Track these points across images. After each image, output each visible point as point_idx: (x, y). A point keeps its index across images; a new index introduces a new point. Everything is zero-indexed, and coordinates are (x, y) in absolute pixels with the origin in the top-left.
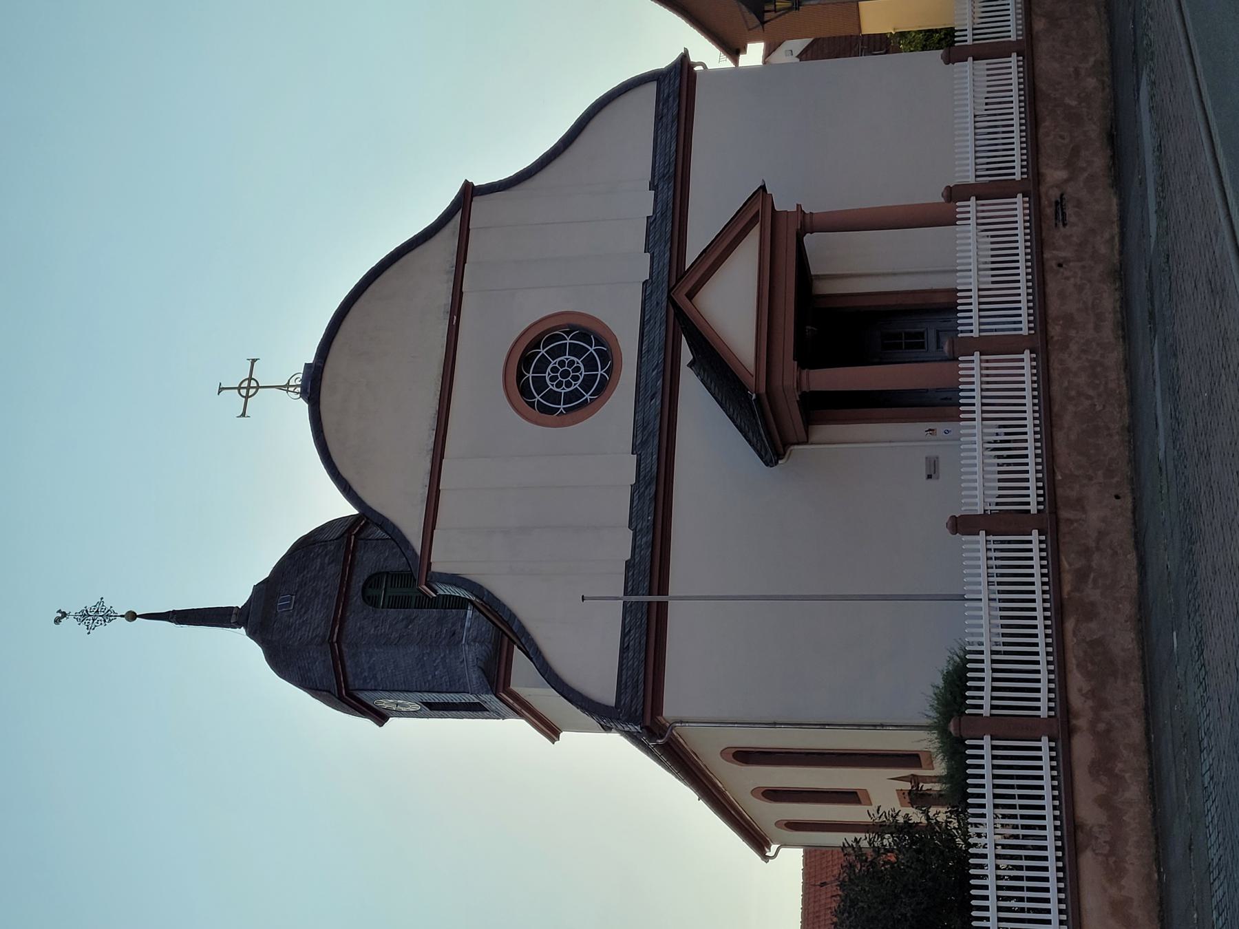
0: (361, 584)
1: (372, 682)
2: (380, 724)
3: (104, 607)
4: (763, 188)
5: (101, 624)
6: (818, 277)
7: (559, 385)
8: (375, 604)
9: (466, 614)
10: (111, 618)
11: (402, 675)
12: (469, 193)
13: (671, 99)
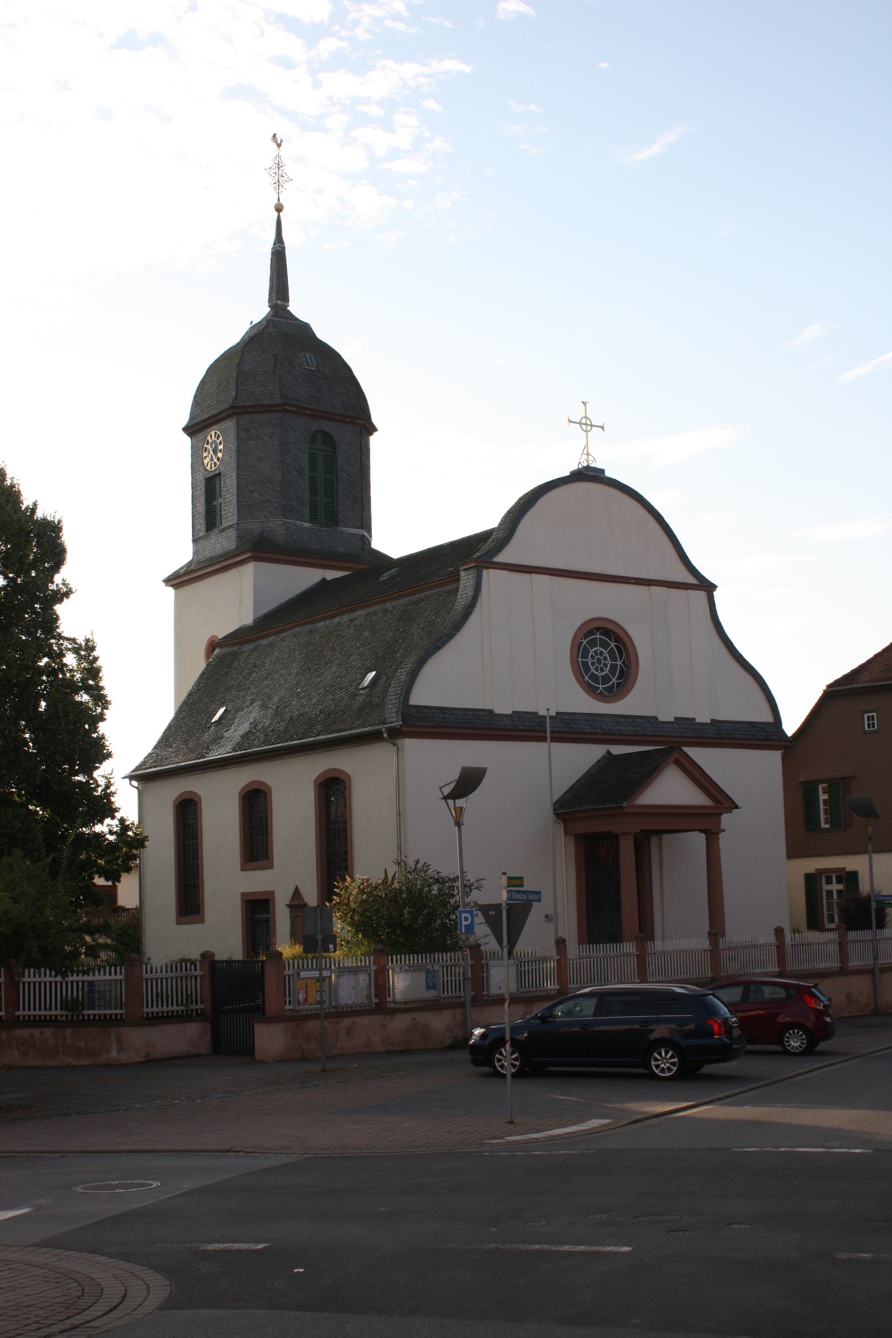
0: (327, 429)
1: (245, 436)
2: (186, 429)
3: (272, 167)
4: (737, 807)
5: (272, 180)
6: (660, 840)
7: (593, 657)
8: (313, 440)
9: (306, 522)
10: (277, 189)
11: (252, 463)
12: (708, 587)
13: (764, 734)
